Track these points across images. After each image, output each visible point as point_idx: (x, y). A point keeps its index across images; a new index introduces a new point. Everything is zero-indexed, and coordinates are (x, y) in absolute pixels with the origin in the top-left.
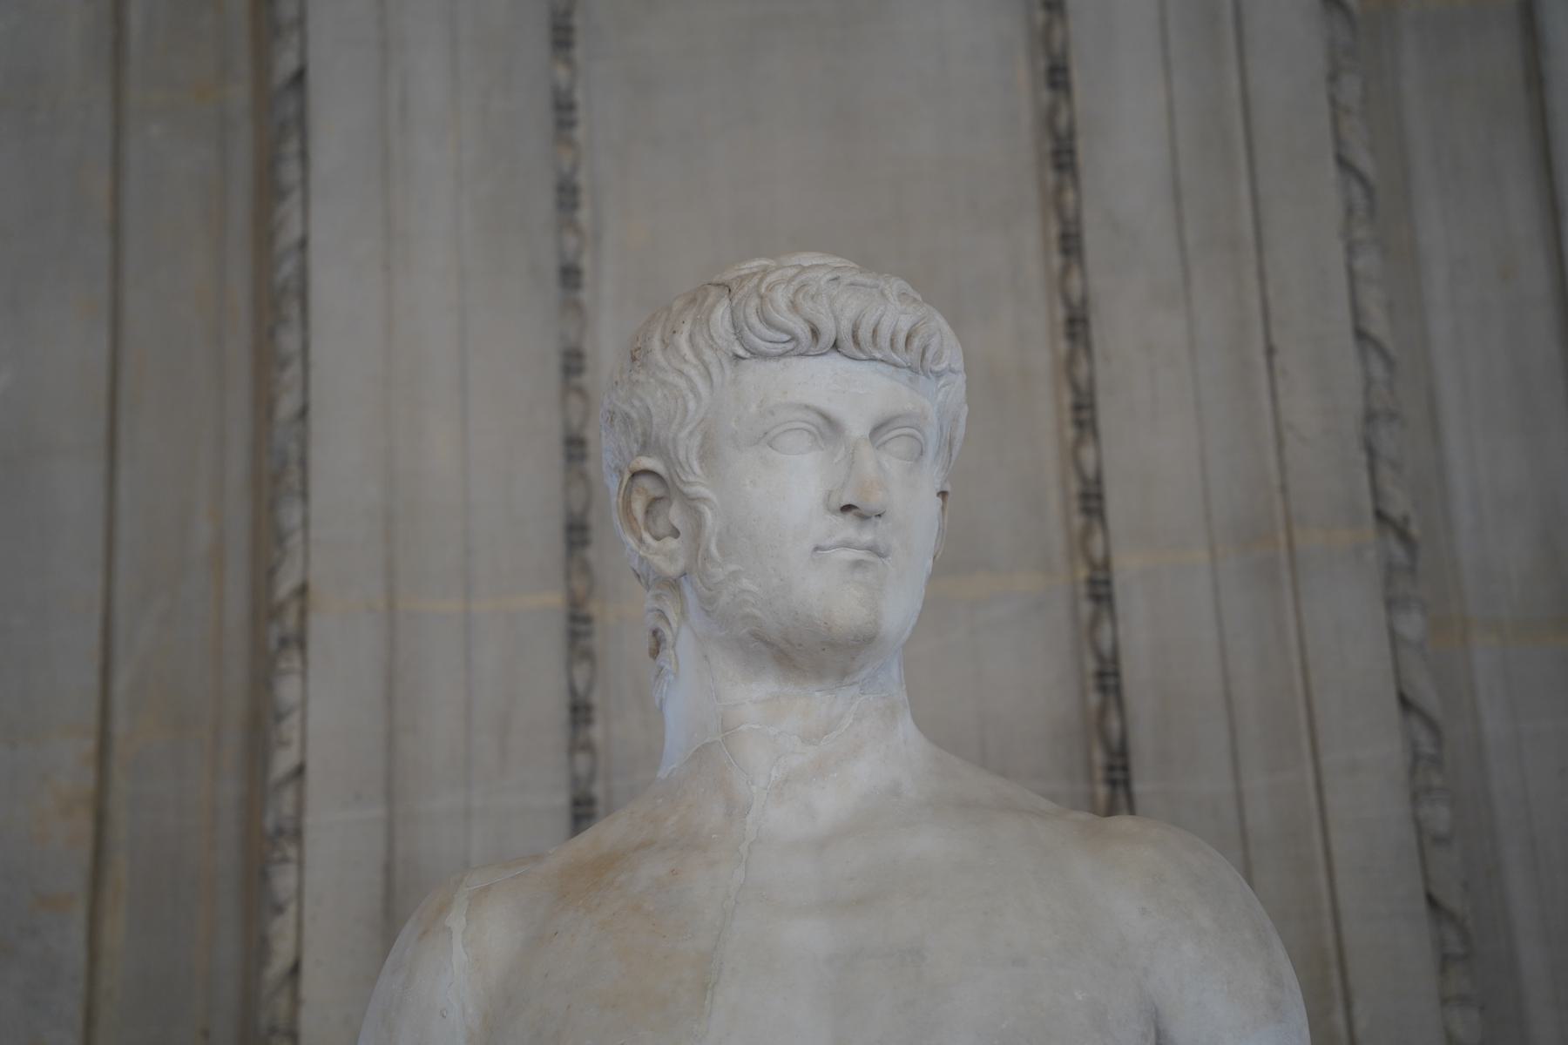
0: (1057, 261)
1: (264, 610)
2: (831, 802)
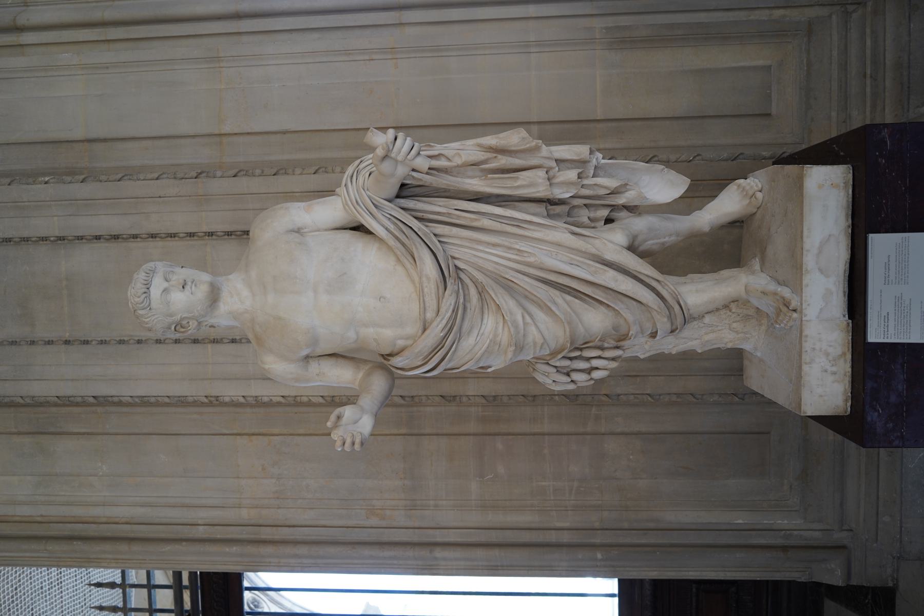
1: (210, 404)
2: (245, 293)
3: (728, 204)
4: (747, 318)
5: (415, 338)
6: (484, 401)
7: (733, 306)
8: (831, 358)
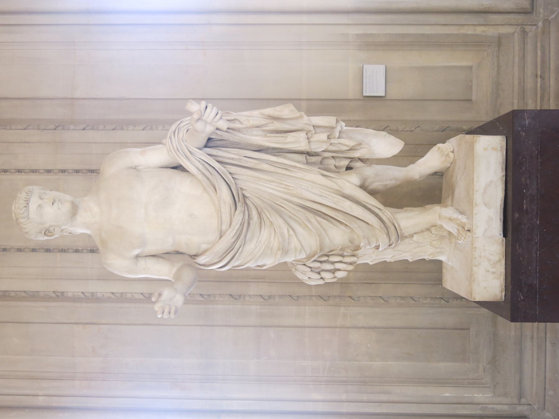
0: (8, 173)
3: (431, 162)
4: (442, 237)
5: (214, 244)
6: (261, 300)
7: (433, 229)
8: (491, 262)
